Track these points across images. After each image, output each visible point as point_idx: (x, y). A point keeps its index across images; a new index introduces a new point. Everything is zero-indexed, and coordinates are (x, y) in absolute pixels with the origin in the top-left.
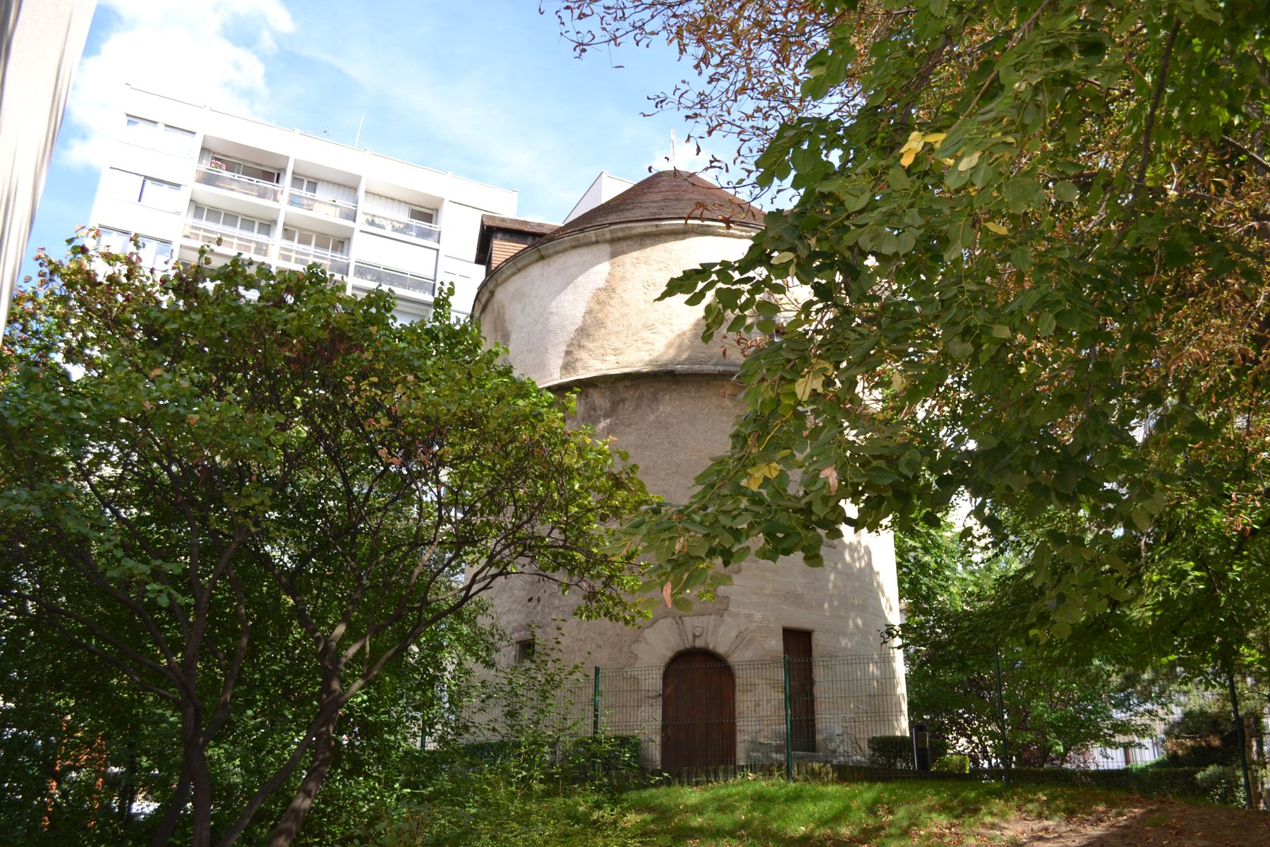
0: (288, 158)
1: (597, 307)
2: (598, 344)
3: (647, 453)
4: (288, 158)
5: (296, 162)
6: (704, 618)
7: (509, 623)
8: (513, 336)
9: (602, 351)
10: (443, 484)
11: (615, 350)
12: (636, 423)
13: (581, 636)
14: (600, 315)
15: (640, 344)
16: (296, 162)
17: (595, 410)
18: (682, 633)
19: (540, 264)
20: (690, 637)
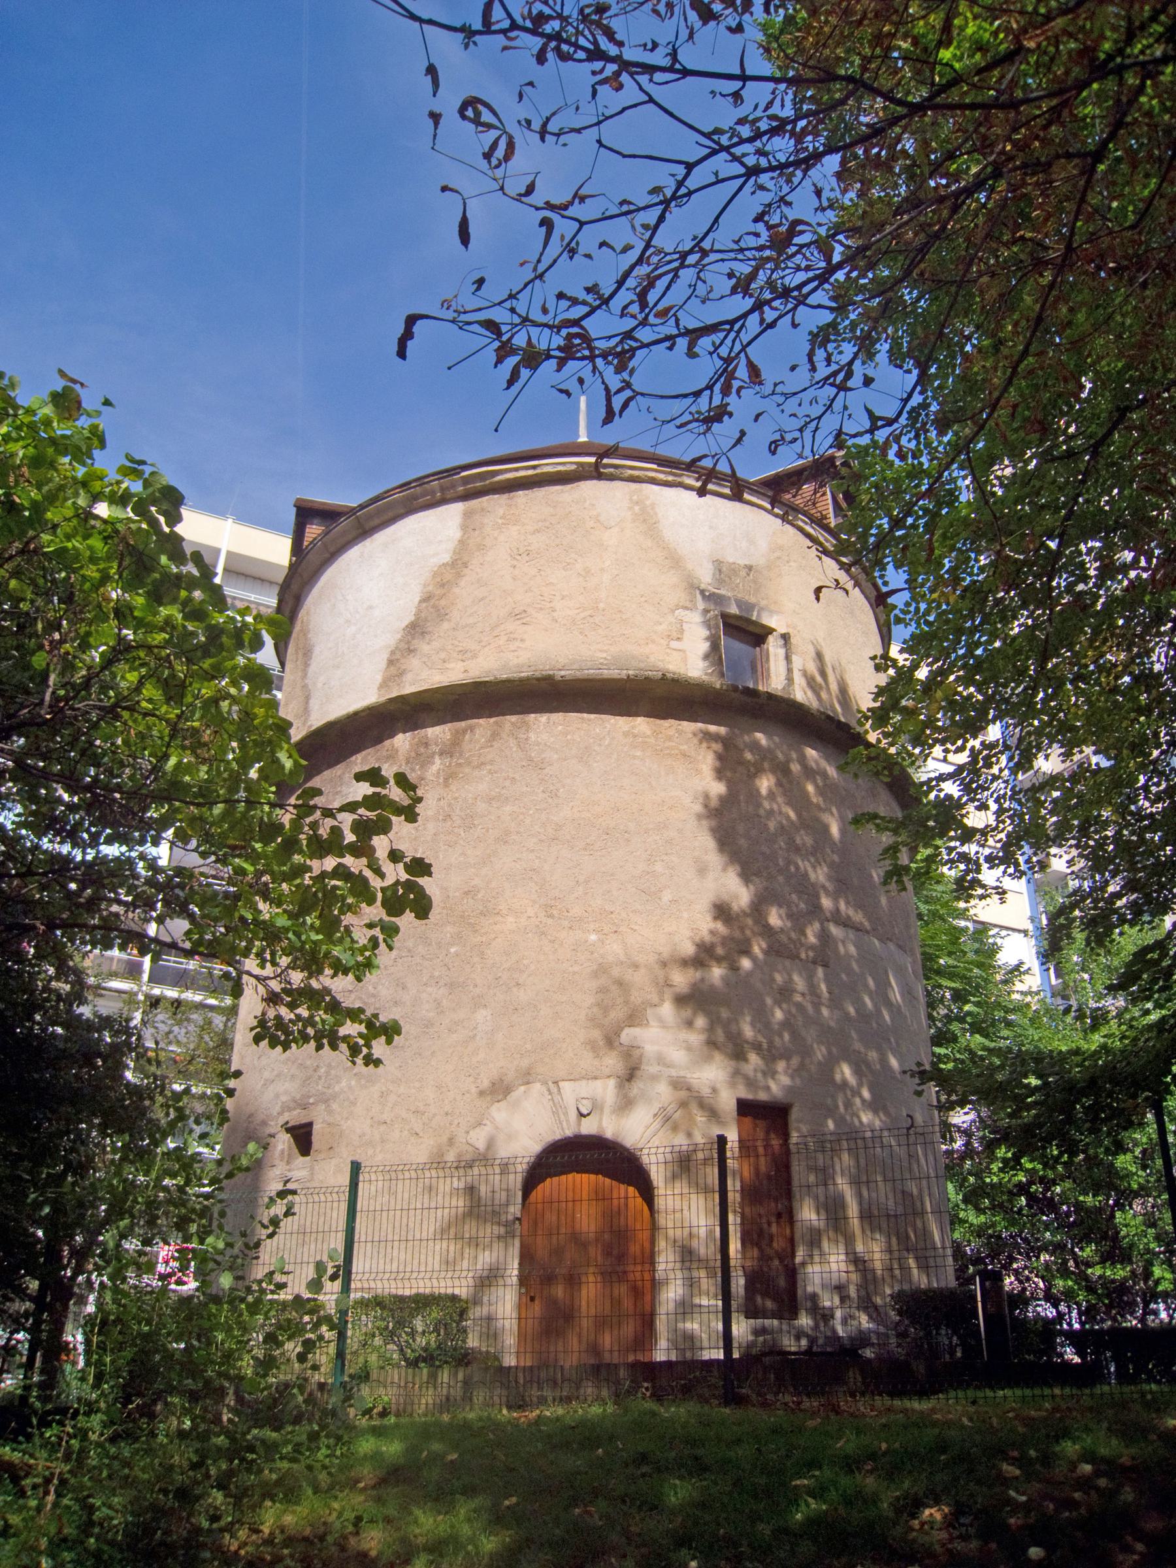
0: (217, 551)
1: (439, 592)
2: (436, 644)
3: (508, 809)
4: (217, 551)
5: (229, 553)
6: (598, 1083)
7: (277, 1096)
8: (317, 651)
9: (443, 655)
10: (1023, 179)
11: (463, 652)
12: (491, 762)
13: (386, 1116)
14: (443, 602)
15: (502, 641)
16: (229, 553)
17: (426, 745)
18: (557, 1109)
19: (409, 618)
20: (573, 1115)
